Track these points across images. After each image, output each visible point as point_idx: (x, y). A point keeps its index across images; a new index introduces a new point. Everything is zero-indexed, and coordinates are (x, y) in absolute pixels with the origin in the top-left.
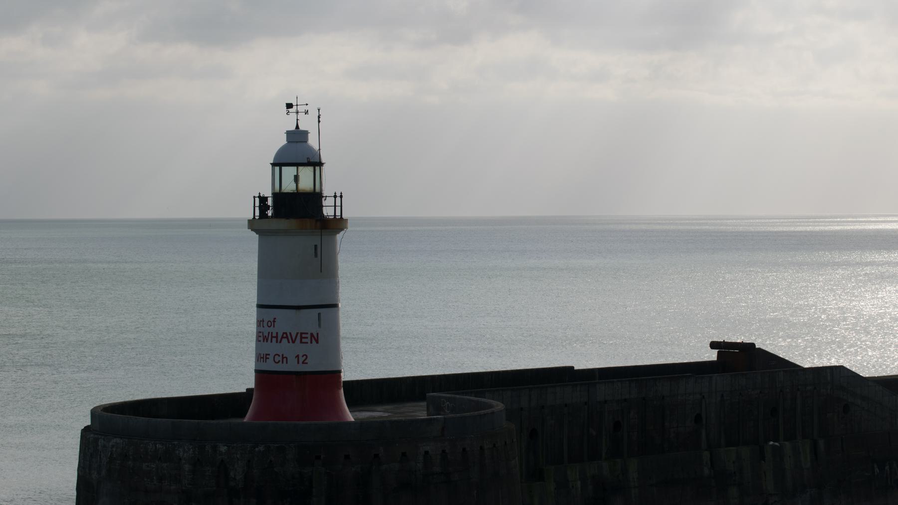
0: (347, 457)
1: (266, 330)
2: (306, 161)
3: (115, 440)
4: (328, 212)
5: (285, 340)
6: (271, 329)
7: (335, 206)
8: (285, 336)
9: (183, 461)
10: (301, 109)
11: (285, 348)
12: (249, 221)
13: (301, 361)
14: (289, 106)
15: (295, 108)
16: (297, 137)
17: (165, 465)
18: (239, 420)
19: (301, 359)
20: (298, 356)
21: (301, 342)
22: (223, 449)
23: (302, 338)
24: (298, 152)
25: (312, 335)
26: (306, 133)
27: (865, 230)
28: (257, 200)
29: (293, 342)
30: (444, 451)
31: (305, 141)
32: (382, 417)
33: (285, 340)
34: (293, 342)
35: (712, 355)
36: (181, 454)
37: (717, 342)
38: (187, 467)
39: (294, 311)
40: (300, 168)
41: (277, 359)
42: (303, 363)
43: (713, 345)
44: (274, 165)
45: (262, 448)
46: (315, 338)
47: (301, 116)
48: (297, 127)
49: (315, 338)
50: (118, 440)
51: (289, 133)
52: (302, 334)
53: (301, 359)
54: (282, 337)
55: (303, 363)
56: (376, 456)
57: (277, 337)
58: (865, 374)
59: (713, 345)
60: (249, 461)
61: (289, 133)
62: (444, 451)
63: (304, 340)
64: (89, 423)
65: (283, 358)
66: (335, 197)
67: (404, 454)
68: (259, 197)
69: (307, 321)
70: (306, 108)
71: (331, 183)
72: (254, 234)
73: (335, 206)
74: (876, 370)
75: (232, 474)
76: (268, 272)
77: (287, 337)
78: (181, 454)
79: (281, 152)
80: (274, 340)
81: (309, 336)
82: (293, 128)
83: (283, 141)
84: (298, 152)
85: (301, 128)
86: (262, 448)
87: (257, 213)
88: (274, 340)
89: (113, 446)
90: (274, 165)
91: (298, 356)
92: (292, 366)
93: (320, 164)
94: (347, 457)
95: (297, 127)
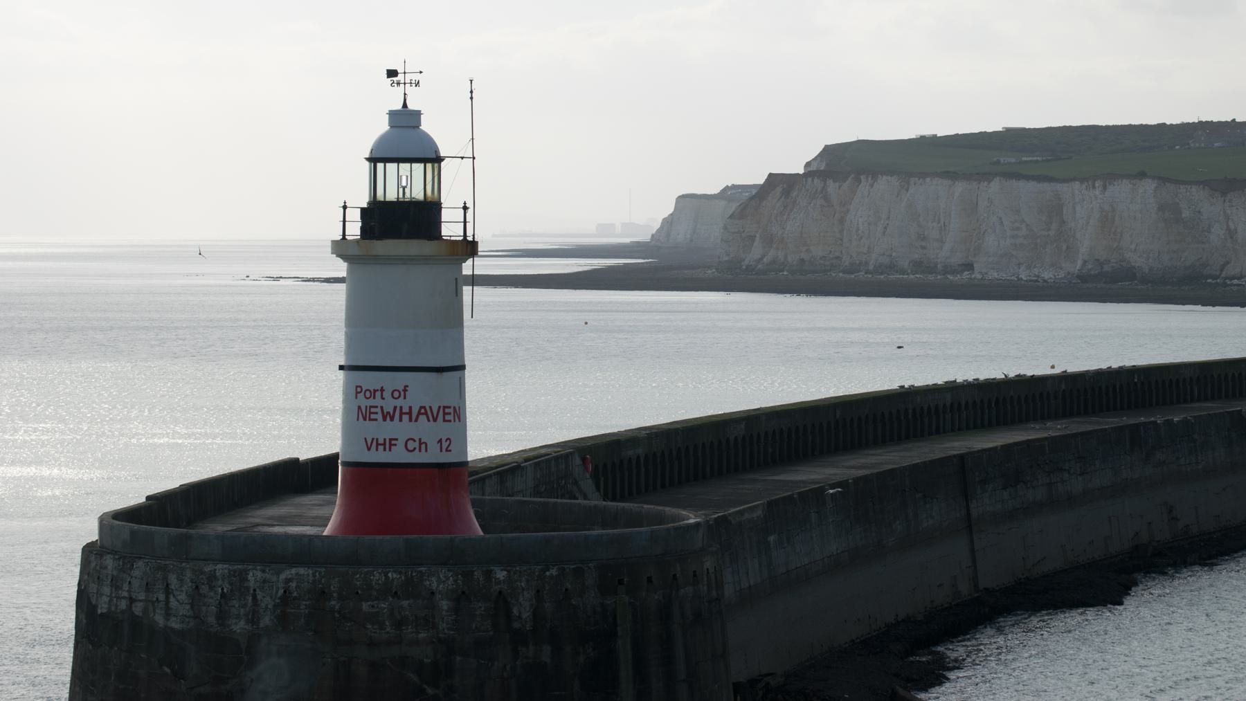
0: (650, 580)
1: (364, 403)
3: (294, 571)
4: (451, 229)
5: (423, 418)
6: (399, 403)
7: (465, 222)
8: (423, 411)
9: (438, 596)
11: (400, 429)
12: (334, 243)
14: (392, 73)
16: (405, 120)
17: (405, 603)
19: (445, 445)
20: (440, 441)
21: (445, 421)
22: (501, 574)
23: (445, 414)
24: (405, 141)
26: (418, 114)
29: (435, 420)
31: (417, 125)
32: (341, 506)
33: (423, 418)
38: (445, 604)
39: (434, 374)
40: (414, 165)
41: (411, 445)
44: (373, 160)
45: (554, 572)
48: (405, 105)
50: (302, 571)
51: (392, 114)
54: (419, 413)
57: (410, 413)
61: (392, 114)
63: (447, 417)
64: (95, 537)
65: (420, 444)
69: (421, 390)
71: (453, 192)
72: (340, 261)
73: (465, 222)
74: (333, 411)
75: (515, 611)
76: (361, 317)
77: (426, 413)
78: (434, 585)
79: (382, 141)
80: (406, 418)
81: (451, 410)
82: (399, 106)
83: (383, 126)
84: (405, 141)
85: (411, 106)
86: (554, 572)
88: (406, 418)
89: (288, 581)
90: (373, 160)
91: (440, 441)
93: (438, 160)
94: (650, 580)
95: (405, 105)
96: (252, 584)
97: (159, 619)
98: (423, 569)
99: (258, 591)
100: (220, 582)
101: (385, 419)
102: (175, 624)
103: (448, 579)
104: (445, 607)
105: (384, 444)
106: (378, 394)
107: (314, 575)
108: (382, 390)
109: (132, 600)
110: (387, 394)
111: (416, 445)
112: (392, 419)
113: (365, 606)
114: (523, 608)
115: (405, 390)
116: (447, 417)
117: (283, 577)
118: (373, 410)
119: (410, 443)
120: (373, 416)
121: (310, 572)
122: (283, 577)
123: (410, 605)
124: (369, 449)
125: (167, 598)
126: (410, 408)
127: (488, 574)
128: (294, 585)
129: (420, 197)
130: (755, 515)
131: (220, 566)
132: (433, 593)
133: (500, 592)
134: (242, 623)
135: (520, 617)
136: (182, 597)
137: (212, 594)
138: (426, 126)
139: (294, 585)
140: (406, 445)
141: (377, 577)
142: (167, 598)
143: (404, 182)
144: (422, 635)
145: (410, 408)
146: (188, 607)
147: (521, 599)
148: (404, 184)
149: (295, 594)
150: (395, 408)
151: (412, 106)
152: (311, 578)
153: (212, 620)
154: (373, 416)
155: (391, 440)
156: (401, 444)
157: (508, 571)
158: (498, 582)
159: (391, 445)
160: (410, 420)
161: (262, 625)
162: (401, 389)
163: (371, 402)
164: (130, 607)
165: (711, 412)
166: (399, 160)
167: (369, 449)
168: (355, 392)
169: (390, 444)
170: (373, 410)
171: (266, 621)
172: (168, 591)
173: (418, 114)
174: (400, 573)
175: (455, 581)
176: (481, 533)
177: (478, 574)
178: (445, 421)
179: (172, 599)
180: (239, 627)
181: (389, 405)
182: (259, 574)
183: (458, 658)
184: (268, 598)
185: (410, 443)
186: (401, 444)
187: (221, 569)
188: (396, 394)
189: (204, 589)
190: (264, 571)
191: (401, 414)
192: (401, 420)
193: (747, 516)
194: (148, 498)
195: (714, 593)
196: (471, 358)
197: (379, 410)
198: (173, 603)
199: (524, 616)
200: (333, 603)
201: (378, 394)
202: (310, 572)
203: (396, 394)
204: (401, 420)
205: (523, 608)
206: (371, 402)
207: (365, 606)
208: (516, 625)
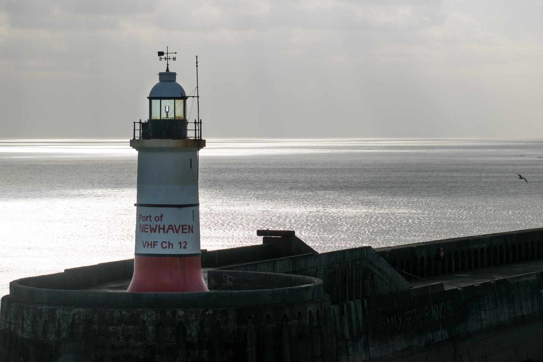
2: (180, 96)
3: (77, 310)
4: (191, 134)
5: (170, 231)
6: (159, 223)
7: (196, 130)
8: (171, 227)
10: (171, 56)
11: (160, 237)
13: (182, 247)
14: (161, 54)
15: (165, 55)
16: (168, 77)
17: (130, 327)
18: (124, 291)
19: (183, 245)
20: (180, 243)
21: (183, 232)
22: (181, 313)
23: (183, 229)
24: (168, 87)
25: (189, 226)
26: (174, 74)
27: (10, 159)
28: (138, 126)
29: (177, 232)
30: (317, 310)
33: (170, 231)
34: (177, 232)
35: (259, 241)
36: (146, 318)
37: (263, 231)
38: (151, 328)
40: (177, 101)
42: (184, 248)
43: (260, 233)
45: (210, 312)
46: (191, 229)
47: (171, 62)
48: (168, 70)
49: (191, 229)
50: (81, 310)
51: (161, 74)
52: (183, 226)
53: (183, 245)
54: (169, 229)
55: (184, 248)
56: (285, 315)
57: (164, 229)
58: (320, 252)
59: (260, 233)
60: (201, 322)
61: (161, 74)
62: (317, 310)
63: (184, 231)
65: (169, 244)
66: (195, 123)
67: (300, 313)
68: (140, 122)
70: (174, 55)
73: (196, 130)
75: (188, 332)
79: (155, 89)
81: (187, 227)
82: (164, 71)
83: (157, 81)
84: (168, 87)
87: (138, 134)
89: (74, 315)
91: (180, 243)
92: (176, 250)
93: (184, 98)
94: (268, 316)
95: (168, 70)
96: (58, 316)
97: (19, 333)
98: (140, 310)
99: (61, 320)
100: (44, 315)
101: (151, 232)
102: (26, 337)
103: (152, 315)
104: (151, 330)
105: (151, 244)
106: (149, 218)
107: (86, 312)
108: (150, 217)
109: (11, 323)
110: (153, 219)
111: (167, 245)
112: (155, 232)
113: (111, 328)
114: (193, 331)
115: (161, 217)
116: (184, 231)
117: (72, 312)
118: (146, 227)
119: (164, 244)
120: (146, 230)
121: (85, 310)
122: (72, 312)
123: (132, 328)
124: (144, 247)
125: (23, 322)
126: (164, 226)
127: (174, 313)
128: (77, 317)
129: (171, 116)
130: (530, 279)
131: (44, 307)
132: (145, 322)
133: (180, 322)
134: (53, 336)
135: (191, 335)
136: (29, 322)
137: (41, 321)
138: (178, 80)
139: (77, 317)
140: (171, 245)
141: (117, 313)
142: (23, 322)
143: (167, 109)
144: (139, 344)
145: (164, 226)
146: (31, 327)
147: (192, 326)
148: (167, 110)
149: (77, 322)
150: (156, 226)
151: (171, 70)
152: (85, 314)
153: (40, 334)
154: (146, 230)
155: (154, 242)
156: (159, 244)
157: (185, 311)
158: (180, 317)
159: (154, 245)
160: (164, 232)
161: (62, 337)
162: (159, 216)
163: (146, 223)
164: (10, 327)
165: (521, 228)
166: (161, 98)
167: (144, 247)
168: (139, 217)
169: (154, 244)
170: (146, 227)
171: (64, 335)
172: (23, 320)
173: (174, 74)
174: (128, 312)
175: (157, 316)
176: (208, 290)
177: (168, 313)
178: (183, 232)
179: (25, 323)
180: (52, 338)
181: (154, 224)
182: (61, 311)
183: (157, 356)
184: (65, 324)
185: (164, 244)
186: (159, 244)
187: (45, 308)
188: (157, 219)
189: (38, 318)
190: (63, 310)
191: (160, 229)
192: (159, 232)
193: (523, 279)
194: (66, 270)
195: (315, 324)
196: (200, 202)
197: (149, 227)
198: (25, 325)
199: (193, 335)
200: (95, 326)
201: (149, 218)
202: (85, 310)
203: (157, 219)
204: (159, 232)
205: (193, 331)
206: (146, 223)
207: (111, 328)
208: (189, 339)
